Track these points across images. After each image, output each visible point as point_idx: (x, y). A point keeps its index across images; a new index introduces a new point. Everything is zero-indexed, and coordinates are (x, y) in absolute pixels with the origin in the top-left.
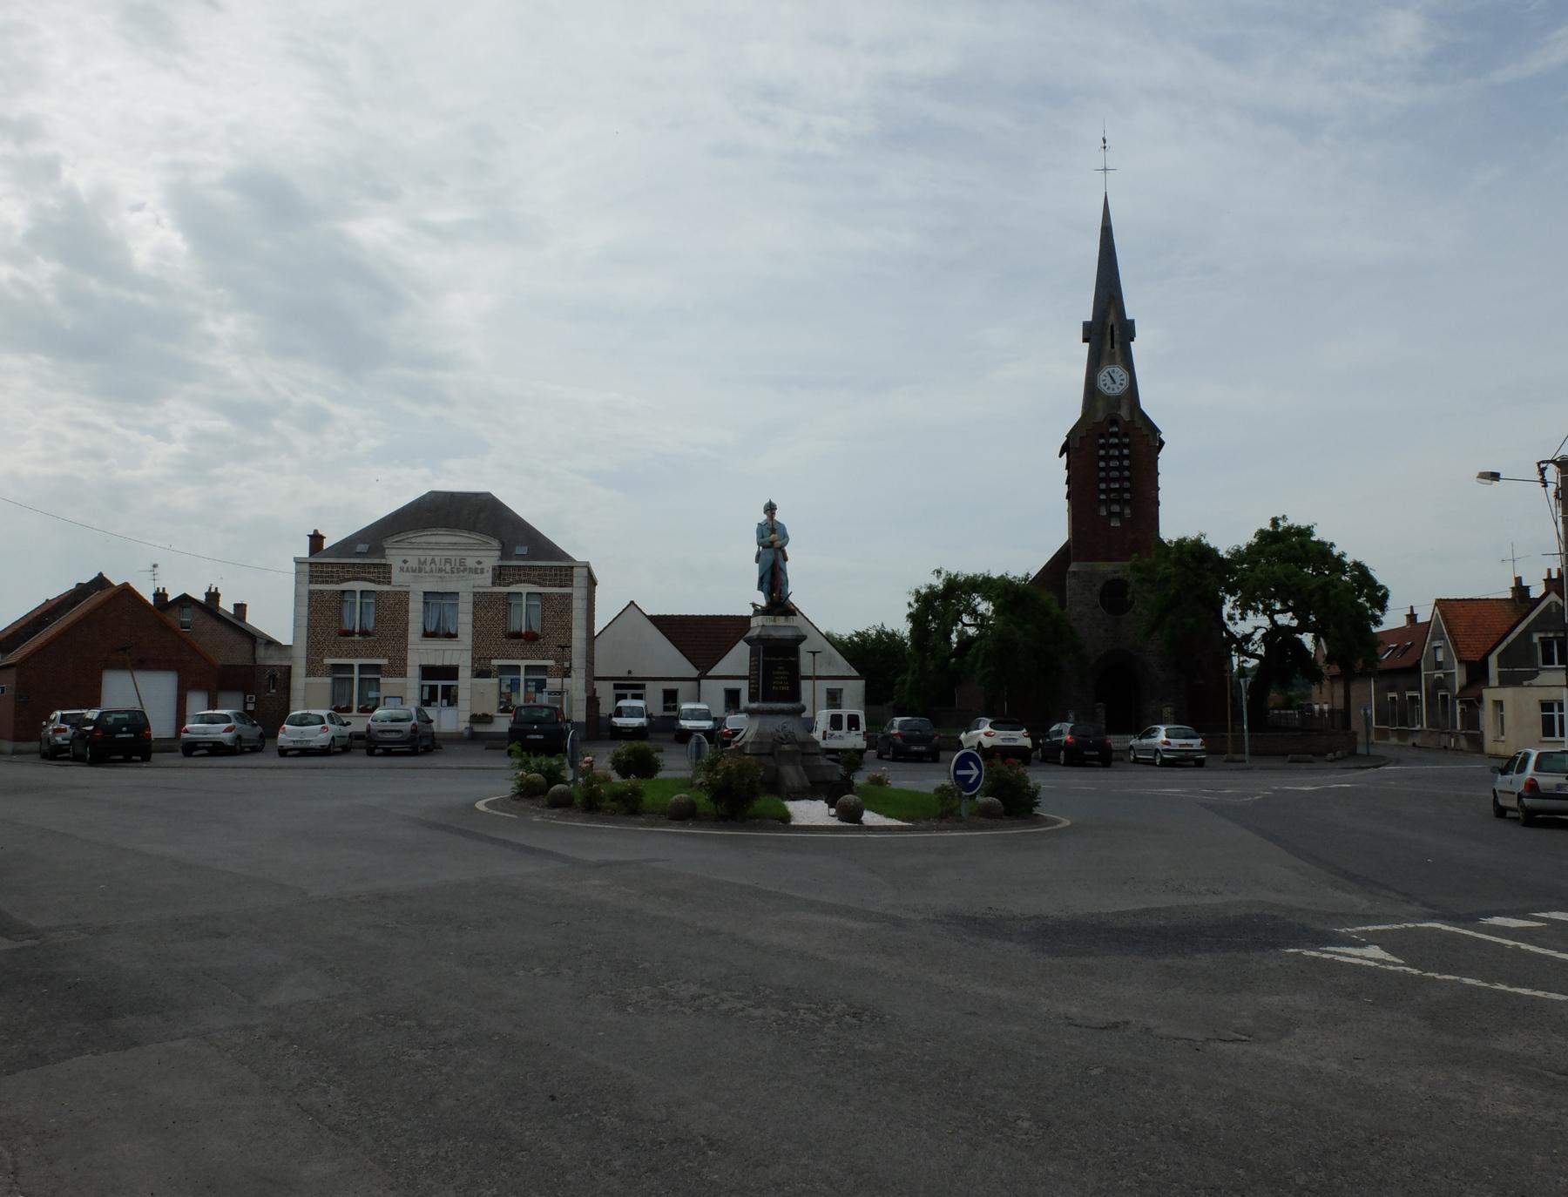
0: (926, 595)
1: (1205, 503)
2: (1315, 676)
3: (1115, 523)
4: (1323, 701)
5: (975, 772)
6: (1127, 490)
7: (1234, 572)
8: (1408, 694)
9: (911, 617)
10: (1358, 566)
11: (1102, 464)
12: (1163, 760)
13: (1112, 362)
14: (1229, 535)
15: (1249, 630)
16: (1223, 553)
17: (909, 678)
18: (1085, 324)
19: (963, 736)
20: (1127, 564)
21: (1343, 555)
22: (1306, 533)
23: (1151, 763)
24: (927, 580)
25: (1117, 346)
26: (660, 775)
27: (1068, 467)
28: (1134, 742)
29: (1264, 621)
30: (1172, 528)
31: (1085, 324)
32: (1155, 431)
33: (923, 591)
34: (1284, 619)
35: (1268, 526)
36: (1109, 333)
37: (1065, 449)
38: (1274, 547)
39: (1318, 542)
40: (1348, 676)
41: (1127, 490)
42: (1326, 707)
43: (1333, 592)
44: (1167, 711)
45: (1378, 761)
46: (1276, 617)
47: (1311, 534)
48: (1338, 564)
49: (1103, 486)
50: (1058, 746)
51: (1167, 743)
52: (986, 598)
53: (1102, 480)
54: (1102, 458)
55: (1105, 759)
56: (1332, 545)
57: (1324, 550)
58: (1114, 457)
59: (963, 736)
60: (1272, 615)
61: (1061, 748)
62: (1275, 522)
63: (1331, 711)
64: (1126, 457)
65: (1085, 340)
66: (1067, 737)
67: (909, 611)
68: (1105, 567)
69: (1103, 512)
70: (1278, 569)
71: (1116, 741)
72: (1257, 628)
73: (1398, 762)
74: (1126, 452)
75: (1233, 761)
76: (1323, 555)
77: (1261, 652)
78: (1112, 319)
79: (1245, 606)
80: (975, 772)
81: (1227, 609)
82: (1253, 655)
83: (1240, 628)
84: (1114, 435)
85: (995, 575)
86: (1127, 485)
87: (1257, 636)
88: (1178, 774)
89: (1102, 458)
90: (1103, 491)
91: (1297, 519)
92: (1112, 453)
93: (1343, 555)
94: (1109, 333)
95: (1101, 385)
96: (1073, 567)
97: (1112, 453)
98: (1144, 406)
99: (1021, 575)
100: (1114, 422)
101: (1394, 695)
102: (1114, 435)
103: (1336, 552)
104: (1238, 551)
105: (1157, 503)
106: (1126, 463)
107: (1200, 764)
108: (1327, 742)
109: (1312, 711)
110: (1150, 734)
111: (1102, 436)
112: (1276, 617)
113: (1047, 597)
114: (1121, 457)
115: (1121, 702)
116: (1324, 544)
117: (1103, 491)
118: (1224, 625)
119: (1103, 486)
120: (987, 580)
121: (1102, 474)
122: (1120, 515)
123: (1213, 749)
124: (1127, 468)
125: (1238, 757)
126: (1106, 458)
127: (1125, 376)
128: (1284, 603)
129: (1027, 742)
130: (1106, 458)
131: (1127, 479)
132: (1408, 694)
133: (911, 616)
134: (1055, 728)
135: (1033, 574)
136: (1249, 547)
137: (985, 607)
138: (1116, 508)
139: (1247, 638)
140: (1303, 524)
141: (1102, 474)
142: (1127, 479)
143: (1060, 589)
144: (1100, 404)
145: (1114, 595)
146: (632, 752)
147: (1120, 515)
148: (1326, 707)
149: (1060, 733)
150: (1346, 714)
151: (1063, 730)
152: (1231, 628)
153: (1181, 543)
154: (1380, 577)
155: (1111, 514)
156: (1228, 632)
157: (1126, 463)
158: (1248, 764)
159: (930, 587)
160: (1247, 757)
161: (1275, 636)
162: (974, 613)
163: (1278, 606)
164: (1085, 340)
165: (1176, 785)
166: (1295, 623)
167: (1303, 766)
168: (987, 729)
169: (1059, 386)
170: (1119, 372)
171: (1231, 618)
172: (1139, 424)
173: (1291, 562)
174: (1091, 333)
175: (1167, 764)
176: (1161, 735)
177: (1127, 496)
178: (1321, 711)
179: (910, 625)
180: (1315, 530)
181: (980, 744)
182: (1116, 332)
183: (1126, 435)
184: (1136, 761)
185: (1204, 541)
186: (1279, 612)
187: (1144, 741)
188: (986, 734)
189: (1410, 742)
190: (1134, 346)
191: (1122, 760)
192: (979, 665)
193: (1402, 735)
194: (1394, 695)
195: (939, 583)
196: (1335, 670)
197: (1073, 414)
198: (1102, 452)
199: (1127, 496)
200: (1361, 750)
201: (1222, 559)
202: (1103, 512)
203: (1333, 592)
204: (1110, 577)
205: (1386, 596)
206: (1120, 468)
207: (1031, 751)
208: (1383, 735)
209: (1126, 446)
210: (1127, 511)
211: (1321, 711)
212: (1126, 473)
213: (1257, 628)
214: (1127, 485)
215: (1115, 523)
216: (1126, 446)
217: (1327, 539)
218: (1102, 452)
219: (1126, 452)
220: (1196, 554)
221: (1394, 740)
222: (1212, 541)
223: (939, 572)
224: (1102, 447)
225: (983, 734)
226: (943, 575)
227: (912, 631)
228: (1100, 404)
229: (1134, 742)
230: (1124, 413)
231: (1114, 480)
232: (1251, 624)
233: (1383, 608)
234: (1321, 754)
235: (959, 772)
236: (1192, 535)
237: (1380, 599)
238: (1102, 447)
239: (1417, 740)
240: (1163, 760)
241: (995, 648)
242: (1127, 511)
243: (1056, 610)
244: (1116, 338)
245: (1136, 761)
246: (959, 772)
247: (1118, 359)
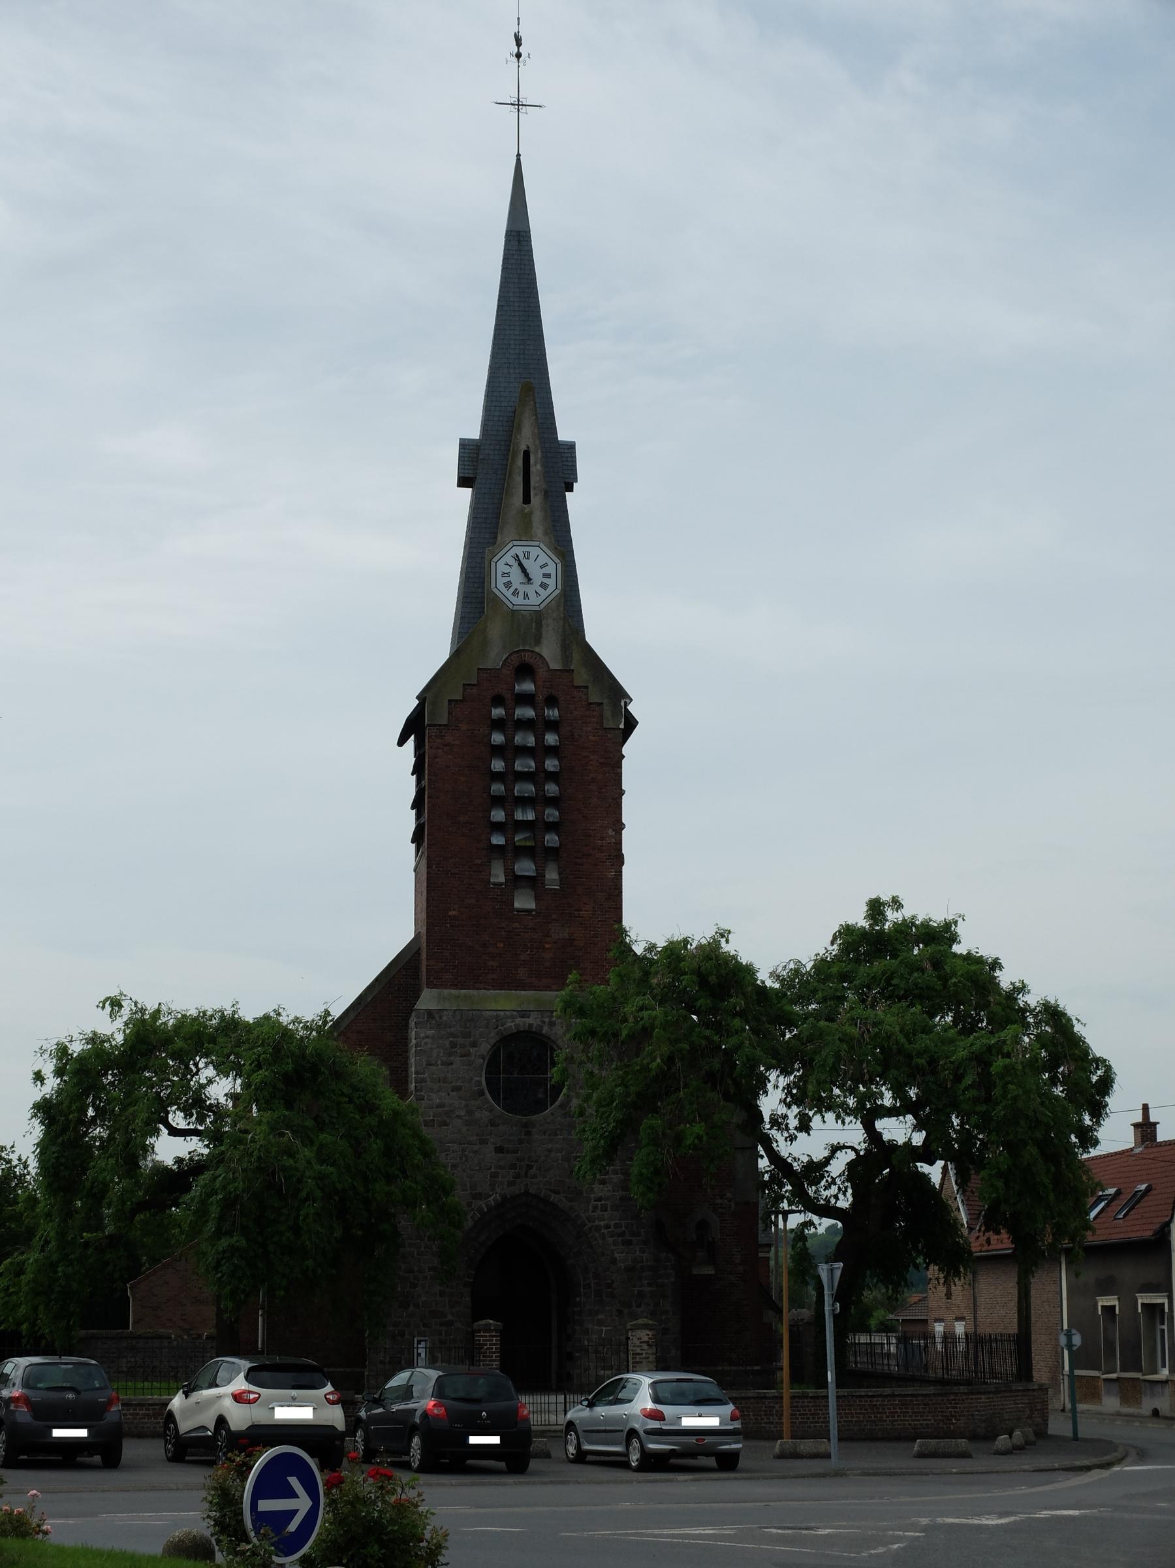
0: (82, 1058)
1: (721, 867)
2: (955, 1259)
3: (524, 901)
4: (953, 1312)
5: (302, 1504)
6: (551, 827)
7: (789, 1021)
8: (1143, 1299)
9: (44, 1109)
10: (1053, 1014)
11: (498, 765)
12: (646, 1455)
13: (525, 533)
14: (781, 935)
15: (819, 1154)
16: (764, 976)
17: (32, 1257)
18: (464, 445)
19: (177, 1402)
20: (555, 998)
21: (1022, 988)
22: (940, 936)
23: (619, 1463)
24: (86, 1022)
25: (536, 500)
26: (242, 1375)
27: (418, 770)
28: (578, 1413)
29: (854, 1134)
30: (658, 906)
31: (464, 445)
32: (617, 694)
33: (76, 1048)
34: (898, 1130)
35: (859, 919)
36: (518, 469)
37: (414, 727)
38: (878, 966)
39: (969, 958)
40: (1027, 1259)
41: (551, 827)
42: (960, 1328)
43: (999, 1063)
44: (640, 1338)
45: (1103, 1454)
46: (880, 1125)
47: (954, 939)
48: (1007, 1008)
49: (498, 815)
50: (404, 1426)
51: (657, 1416)
52: (222, 1069)
53: (498, 801)
54: (498, 751)
55: (516, 1457)
56: (996, 964)
57: (981, 972)
58: (524, 751)
59: (177, 1402)
60: (869, 1116)
61: (413, 1429)
62: (876, 908)
63: (975, 1340)
64: (553, 751)
65: (463, 482)
66: (426, 1403)
67: (37, 1094)
68: (504, 1005)
69: (498, 875)
70: (890, 1017)
71: (543, 1410)
72: (835, 1149)
73: (1142, 1455)
74: (551, 739)
75: (796, 1455)
76: (977, 986)
77: (844, 1203)
78: (526, 438)
79: (809, 1099)
80: (302, 1504)
81: (770, 1103)
82: (827, 1210)
83: (802, 1149)
84: (526, 699)
85: (249, 1014)
86: (552, 814)
87: (837, 1167)
88: (681, 1486)
89: (498, 751)
90: (498, 827)
91: (922, 906)
92: (518, 745)
93: (1022, 988)
94: (518, 469)
95: (498, 584)
96: (428, 1000)
97: (518, 745)
98: (591, 637)
99: (310, 1014)
100: (525, 670)
101: (1112, 1301)
102: (526, 699)
103: (1005, 979)
104: (796, 972)
105: (619, 859)
106: (551, 764)
107: (728, 1463)
108: (974, 1411)
109: (929, 1336)
110: (614, 1393)
111: (498, 701)
112: (880, 1125)
113: (366, 1067)
114: (541, 751)
115: (533, 1317)
116: (980, 961)
117: (498, 827)
118: (767, 1142)
119: (498, 815)
120: (230, 1025)
121: (497, 788)
122: (534, 883)
123: (753, 1426)
124: (552, 777)
125: (807, 1446)
126: (507, 751)
127: (554, 568)
128: (899, 1091)
129: (335, 1416)
130: (507, 751)
131: (553, 802)
132: (1143, 1299)
133: (44, 1109)
134: (400, 1379)
135: (337, 1012)
136: (821, 965)
137: (222, 1089)
138: (526, 867)
139: (815, 1170)
140: (938, 917)
141: (497, 788)
142: (553, 802)
143: (393, 1052)
144: (496, 630)
145: (519, 1069)
146: (1138, 1402)
147: (534, 883)
148: (960, 1328)
149: (407, 1392)
150: (1022, 1342)
151: (419, 1387)
152: (784, 1148)
153: (675, 952)
154: (1098, 1038)
155: (516, 881)
156: (774, 1157)
157: (551, 764)
158: (834, 1463)
159: (94, 1039)
160: (833, 1446)
161: (876, 1163)
162: (197, 1104)
163: (888, 1100)
164: (463, 482)
165: (692, 1515)
166: (918, 1139)
167: (954, 1465)
168: (239, 1384)
169: (398, 586)
170: (540, 560)
171: (777, 1122)
172: (582, 676)
173: (906, 995)
174: (475, 466)
175: (654, 1463)
176: (641, 1396)
177: (551, 839)
178: (948, 1337)
179: (37, 1131)
180: (961, 929)
181: (221, 1421)
182: (536, 468)
183: (551, 701)
184: (581, 1457)
185: (725, 948)
186: (892, 1112)
187: (602, 1411)
188: (238, 1398)
189: (1147, 1405)
190: (572, 500)
191: (547, 1455)
192: (211, 1227)
193: (1130, 1391)
194: (1112, 1301)
195: (114, 1030)
196: (1002, 1242)
197: (432, 647)
198: (498, 738)
199: (551, 839)
200: (1058, 1426)
201: (763, 990)
202: (498, 875)
203: (999, 1063)
204: (510, 1025)
205: (1106, 1084)
206: (538, 777)
207: (342, 1436)
208: (1086, 1390)
209: (553, 726)
210: (552, 875)
211: (948, 1337)
212: (552, 789)
213: (835, 1149)
214: (552, 814)
215: (524, 901)
216: (553, 726)
217: (987, 951)
218: (498, 738)
219: (551, 739)
220: (708, 975)
221: (1111, 1403)
222: (742, 948)
223: (115, 1004)
224: (499, 725)
225: (228, 1396)
226: (125, 1013)
227: (44, 1147)
228: (496, 630)
229: (578, 1413)
230: (549, 651)
231: (524, 802)
232: (827, 1139)
233: (1098, 1111)
234: (984, 1435)
235: (265, 1505)
236: (699, 933)
237: (1091, 1086)
238: (499, 725)
239: (1163, 1403)
240: (646, 1455)
241: (249, 1195)
242: (552, 875)
243: (389, 1100)
244: (535, 480)
245: (581, 1457)
246: (265, 1505)
247: (538, 528)
